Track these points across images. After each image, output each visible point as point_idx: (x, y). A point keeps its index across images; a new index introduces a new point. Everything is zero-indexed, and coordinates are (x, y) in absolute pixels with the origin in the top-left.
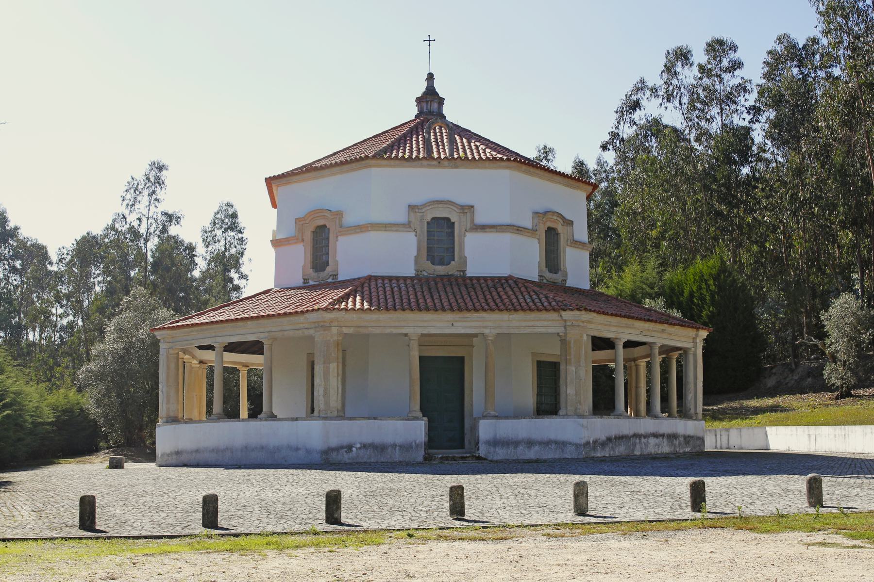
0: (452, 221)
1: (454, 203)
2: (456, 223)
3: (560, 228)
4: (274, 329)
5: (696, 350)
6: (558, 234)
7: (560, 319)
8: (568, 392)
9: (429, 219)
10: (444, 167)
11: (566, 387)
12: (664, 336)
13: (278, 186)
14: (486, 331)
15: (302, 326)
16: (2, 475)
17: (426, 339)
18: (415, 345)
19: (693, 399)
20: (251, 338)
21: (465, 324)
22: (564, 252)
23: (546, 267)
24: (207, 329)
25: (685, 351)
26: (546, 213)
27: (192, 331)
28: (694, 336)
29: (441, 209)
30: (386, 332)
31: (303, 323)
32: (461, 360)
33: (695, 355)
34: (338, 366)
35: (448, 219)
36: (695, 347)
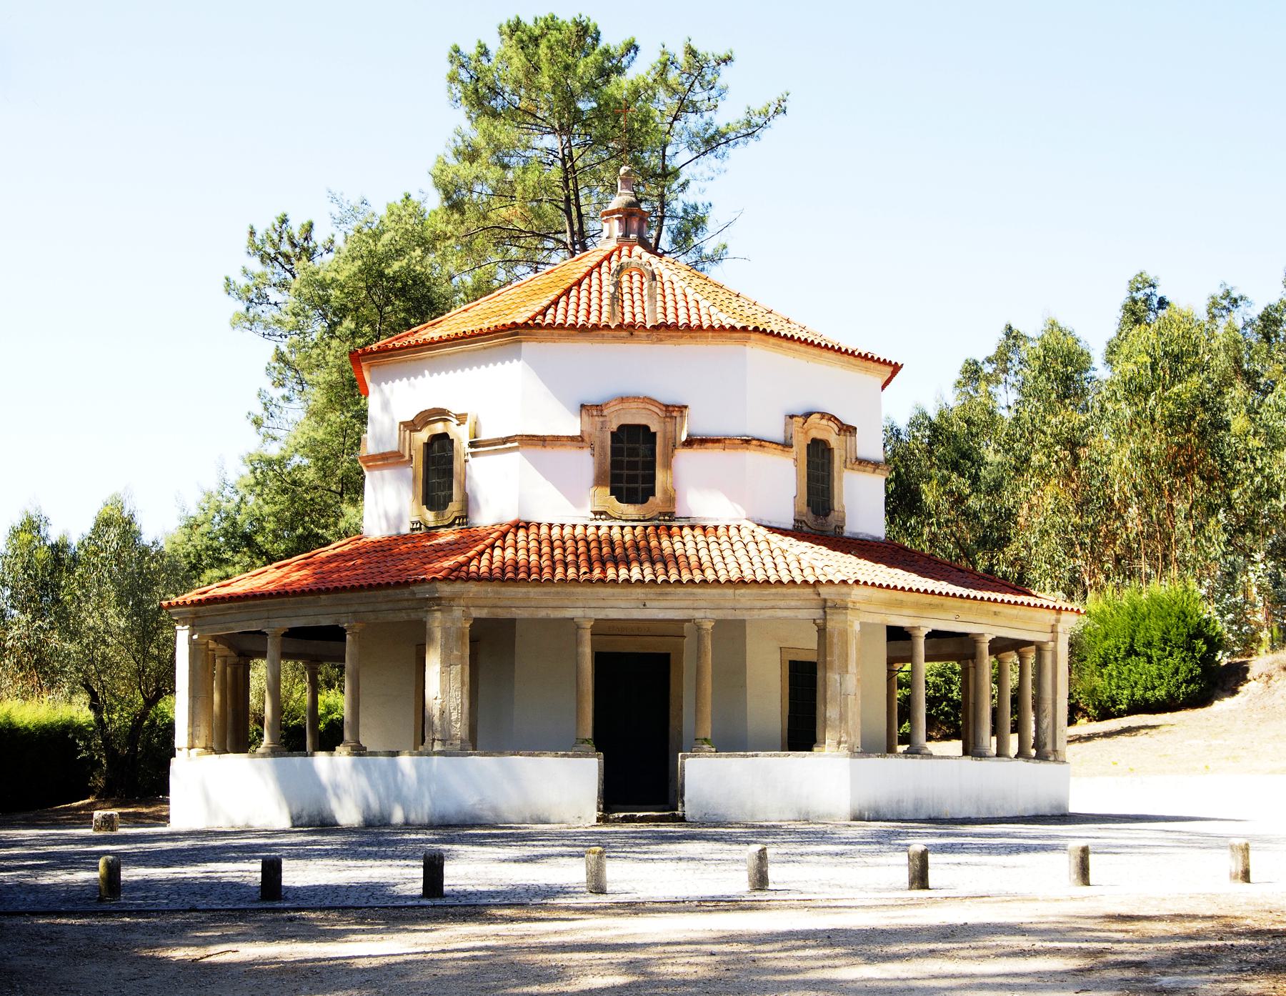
0: (653, 430)
1: (655, 401)
2: (658, 435)
3: (834, 440)
4: (362, 608)
5: (1056, 646)
6: (830, 450)
7: (816, 597)
8: (828, 715)
9: (614, 427)
10: (639, 342)
11: (825, 706)
12: (998, 621)
13: (371, 366)
14: (698, 615)
15: (406, 604)
16: (3, 833)
17: (602, 629)
18: (587, 637)
19: (1051, 725)
20: (326, 622)
21: (663, 604)
22: (841, 479)
23: (808, 505)
24: (255, 606)
25: (1039, 648)
26: (808, 415)
27: (231, 608)
28: (1053, 622)
29: (634, 411)
30: (540, 616)
31: (408, 600)
32: (666, 657)
33: (18, 876)
34: (463, 669)
35: (646, 428)
36: (1055, 640)
